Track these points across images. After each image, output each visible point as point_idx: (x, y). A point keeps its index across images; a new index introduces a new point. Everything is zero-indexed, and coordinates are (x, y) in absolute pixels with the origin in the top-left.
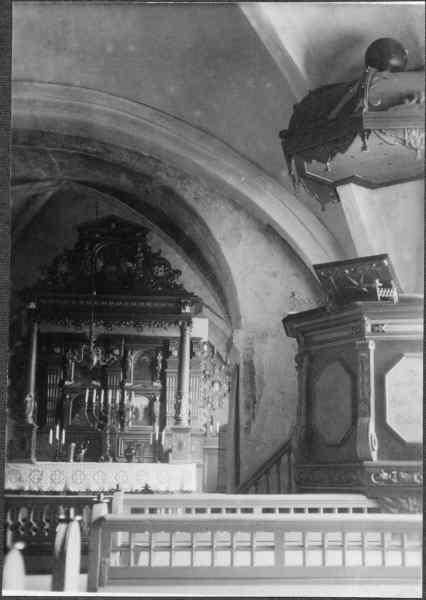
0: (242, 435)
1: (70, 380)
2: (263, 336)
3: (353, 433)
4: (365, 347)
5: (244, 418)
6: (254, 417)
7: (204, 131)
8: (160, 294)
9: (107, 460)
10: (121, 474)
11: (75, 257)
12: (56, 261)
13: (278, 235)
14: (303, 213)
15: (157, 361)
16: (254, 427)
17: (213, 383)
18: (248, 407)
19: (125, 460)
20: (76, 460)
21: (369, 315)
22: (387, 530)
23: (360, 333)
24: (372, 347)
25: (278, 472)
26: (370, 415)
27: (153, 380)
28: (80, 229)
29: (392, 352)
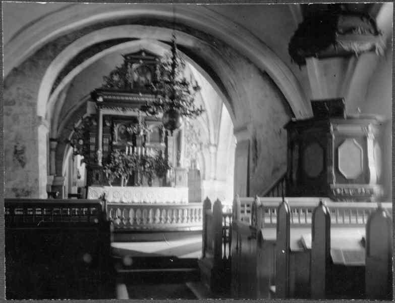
0: (251, 174)
1: (116, 141)
2: (261, 126)
3: (324, 173)
4: (331, 137)
5: (252, 165)
6: (256, 165)
7: (252, 34)
8: (136, 88)
9: (139, 185)
10: (117, 193)
11: (122, 72)
12: (112, 74)
13: (268, 76)
14: (284, 68)
15: (162, 131)
16: (256, 170)
17: (192, 144)
18: (254, 159)
19: (148, 185)
20: (124, 186)
21: (333, 123)
22: (227, 229)
23: (329, 131)
24: (334, 137)
25: (278, 189)
26: (332, 165)
27: (160, 142)
28: (125, 56)
29: (342, 139)
